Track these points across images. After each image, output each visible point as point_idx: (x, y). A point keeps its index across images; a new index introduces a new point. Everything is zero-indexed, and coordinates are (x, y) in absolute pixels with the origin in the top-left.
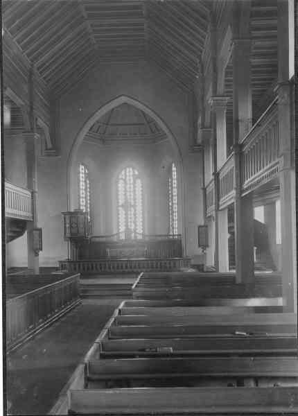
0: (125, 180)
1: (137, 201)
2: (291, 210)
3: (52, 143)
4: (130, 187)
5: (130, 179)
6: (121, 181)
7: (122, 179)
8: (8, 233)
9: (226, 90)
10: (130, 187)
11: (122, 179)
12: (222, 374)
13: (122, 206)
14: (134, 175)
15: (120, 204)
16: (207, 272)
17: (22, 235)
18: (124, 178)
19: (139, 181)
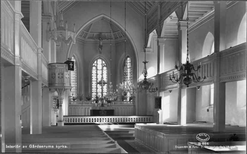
0: (96, 67)
1: (95, 87)
2: (32, 119)
3: (173, 12)
4: (99, 72)
5: (100, 67)
6: (94, 68)
7: (94, 66)
8: (107, 34)
9: (165, 35)
10: (99, 72)
11: (94, 66)
12: (69, 52)
13: (105, 83)
14: (102, 64)
15: (106, 85)
16: (67, 33)
17: (22, 11)
18: (96, 65)
19: (105, 68)
